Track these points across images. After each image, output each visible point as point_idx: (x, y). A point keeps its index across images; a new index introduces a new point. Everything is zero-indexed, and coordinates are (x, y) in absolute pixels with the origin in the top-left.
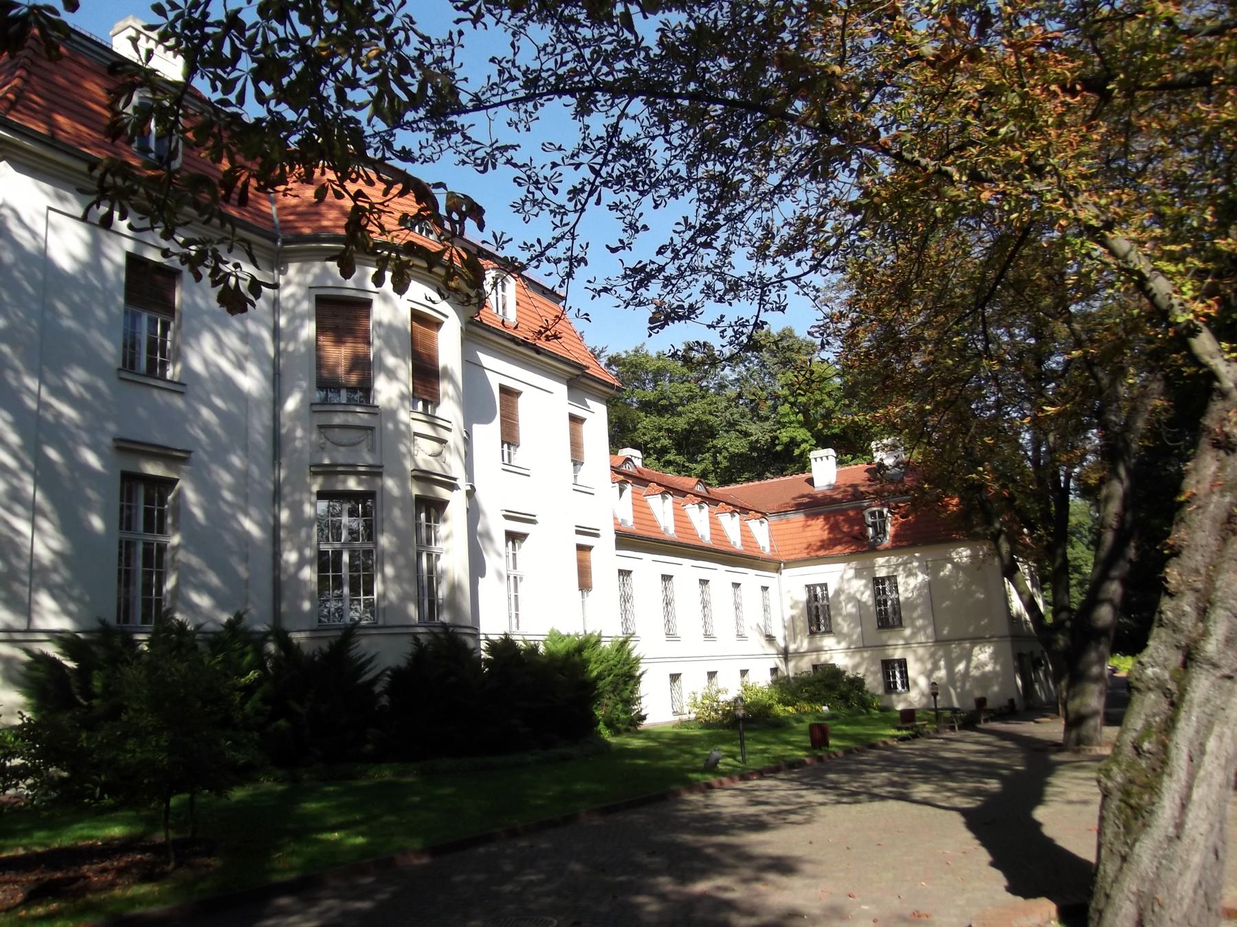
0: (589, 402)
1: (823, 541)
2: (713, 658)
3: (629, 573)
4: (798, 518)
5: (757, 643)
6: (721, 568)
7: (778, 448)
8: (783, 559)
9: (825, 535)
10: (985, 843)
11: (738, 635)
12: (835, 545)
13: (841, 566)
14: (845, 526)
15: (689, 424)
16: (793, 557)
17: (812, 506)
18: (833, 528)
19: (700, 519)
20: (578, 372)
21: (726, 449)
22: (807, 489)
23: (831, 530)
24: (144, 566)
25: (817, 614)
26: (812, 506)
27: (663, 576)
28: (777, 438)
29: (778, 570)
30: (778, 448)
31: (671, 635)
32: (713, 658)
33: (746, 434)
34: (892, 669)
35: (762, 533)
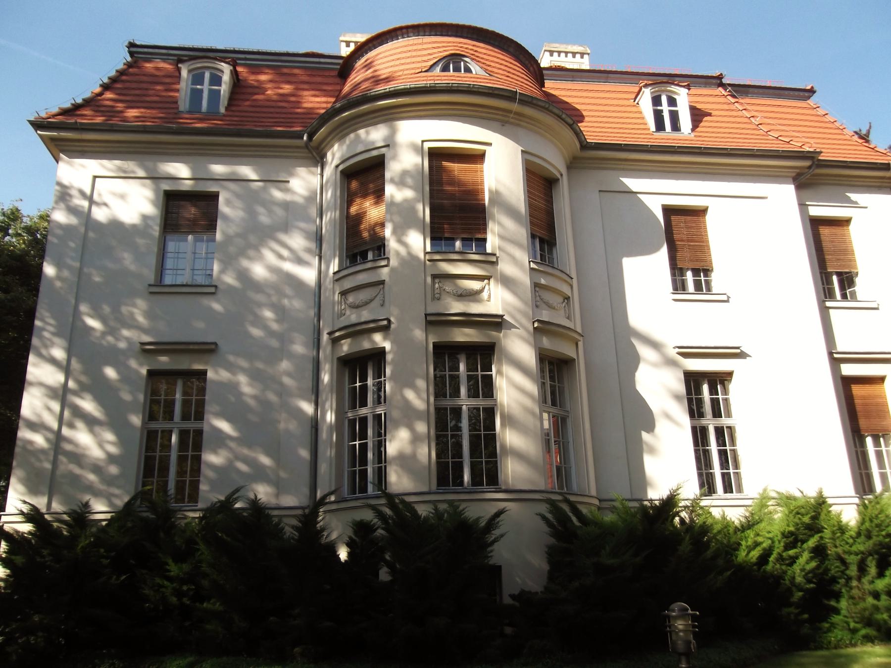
0: (853, 196)
20: (807, 163)
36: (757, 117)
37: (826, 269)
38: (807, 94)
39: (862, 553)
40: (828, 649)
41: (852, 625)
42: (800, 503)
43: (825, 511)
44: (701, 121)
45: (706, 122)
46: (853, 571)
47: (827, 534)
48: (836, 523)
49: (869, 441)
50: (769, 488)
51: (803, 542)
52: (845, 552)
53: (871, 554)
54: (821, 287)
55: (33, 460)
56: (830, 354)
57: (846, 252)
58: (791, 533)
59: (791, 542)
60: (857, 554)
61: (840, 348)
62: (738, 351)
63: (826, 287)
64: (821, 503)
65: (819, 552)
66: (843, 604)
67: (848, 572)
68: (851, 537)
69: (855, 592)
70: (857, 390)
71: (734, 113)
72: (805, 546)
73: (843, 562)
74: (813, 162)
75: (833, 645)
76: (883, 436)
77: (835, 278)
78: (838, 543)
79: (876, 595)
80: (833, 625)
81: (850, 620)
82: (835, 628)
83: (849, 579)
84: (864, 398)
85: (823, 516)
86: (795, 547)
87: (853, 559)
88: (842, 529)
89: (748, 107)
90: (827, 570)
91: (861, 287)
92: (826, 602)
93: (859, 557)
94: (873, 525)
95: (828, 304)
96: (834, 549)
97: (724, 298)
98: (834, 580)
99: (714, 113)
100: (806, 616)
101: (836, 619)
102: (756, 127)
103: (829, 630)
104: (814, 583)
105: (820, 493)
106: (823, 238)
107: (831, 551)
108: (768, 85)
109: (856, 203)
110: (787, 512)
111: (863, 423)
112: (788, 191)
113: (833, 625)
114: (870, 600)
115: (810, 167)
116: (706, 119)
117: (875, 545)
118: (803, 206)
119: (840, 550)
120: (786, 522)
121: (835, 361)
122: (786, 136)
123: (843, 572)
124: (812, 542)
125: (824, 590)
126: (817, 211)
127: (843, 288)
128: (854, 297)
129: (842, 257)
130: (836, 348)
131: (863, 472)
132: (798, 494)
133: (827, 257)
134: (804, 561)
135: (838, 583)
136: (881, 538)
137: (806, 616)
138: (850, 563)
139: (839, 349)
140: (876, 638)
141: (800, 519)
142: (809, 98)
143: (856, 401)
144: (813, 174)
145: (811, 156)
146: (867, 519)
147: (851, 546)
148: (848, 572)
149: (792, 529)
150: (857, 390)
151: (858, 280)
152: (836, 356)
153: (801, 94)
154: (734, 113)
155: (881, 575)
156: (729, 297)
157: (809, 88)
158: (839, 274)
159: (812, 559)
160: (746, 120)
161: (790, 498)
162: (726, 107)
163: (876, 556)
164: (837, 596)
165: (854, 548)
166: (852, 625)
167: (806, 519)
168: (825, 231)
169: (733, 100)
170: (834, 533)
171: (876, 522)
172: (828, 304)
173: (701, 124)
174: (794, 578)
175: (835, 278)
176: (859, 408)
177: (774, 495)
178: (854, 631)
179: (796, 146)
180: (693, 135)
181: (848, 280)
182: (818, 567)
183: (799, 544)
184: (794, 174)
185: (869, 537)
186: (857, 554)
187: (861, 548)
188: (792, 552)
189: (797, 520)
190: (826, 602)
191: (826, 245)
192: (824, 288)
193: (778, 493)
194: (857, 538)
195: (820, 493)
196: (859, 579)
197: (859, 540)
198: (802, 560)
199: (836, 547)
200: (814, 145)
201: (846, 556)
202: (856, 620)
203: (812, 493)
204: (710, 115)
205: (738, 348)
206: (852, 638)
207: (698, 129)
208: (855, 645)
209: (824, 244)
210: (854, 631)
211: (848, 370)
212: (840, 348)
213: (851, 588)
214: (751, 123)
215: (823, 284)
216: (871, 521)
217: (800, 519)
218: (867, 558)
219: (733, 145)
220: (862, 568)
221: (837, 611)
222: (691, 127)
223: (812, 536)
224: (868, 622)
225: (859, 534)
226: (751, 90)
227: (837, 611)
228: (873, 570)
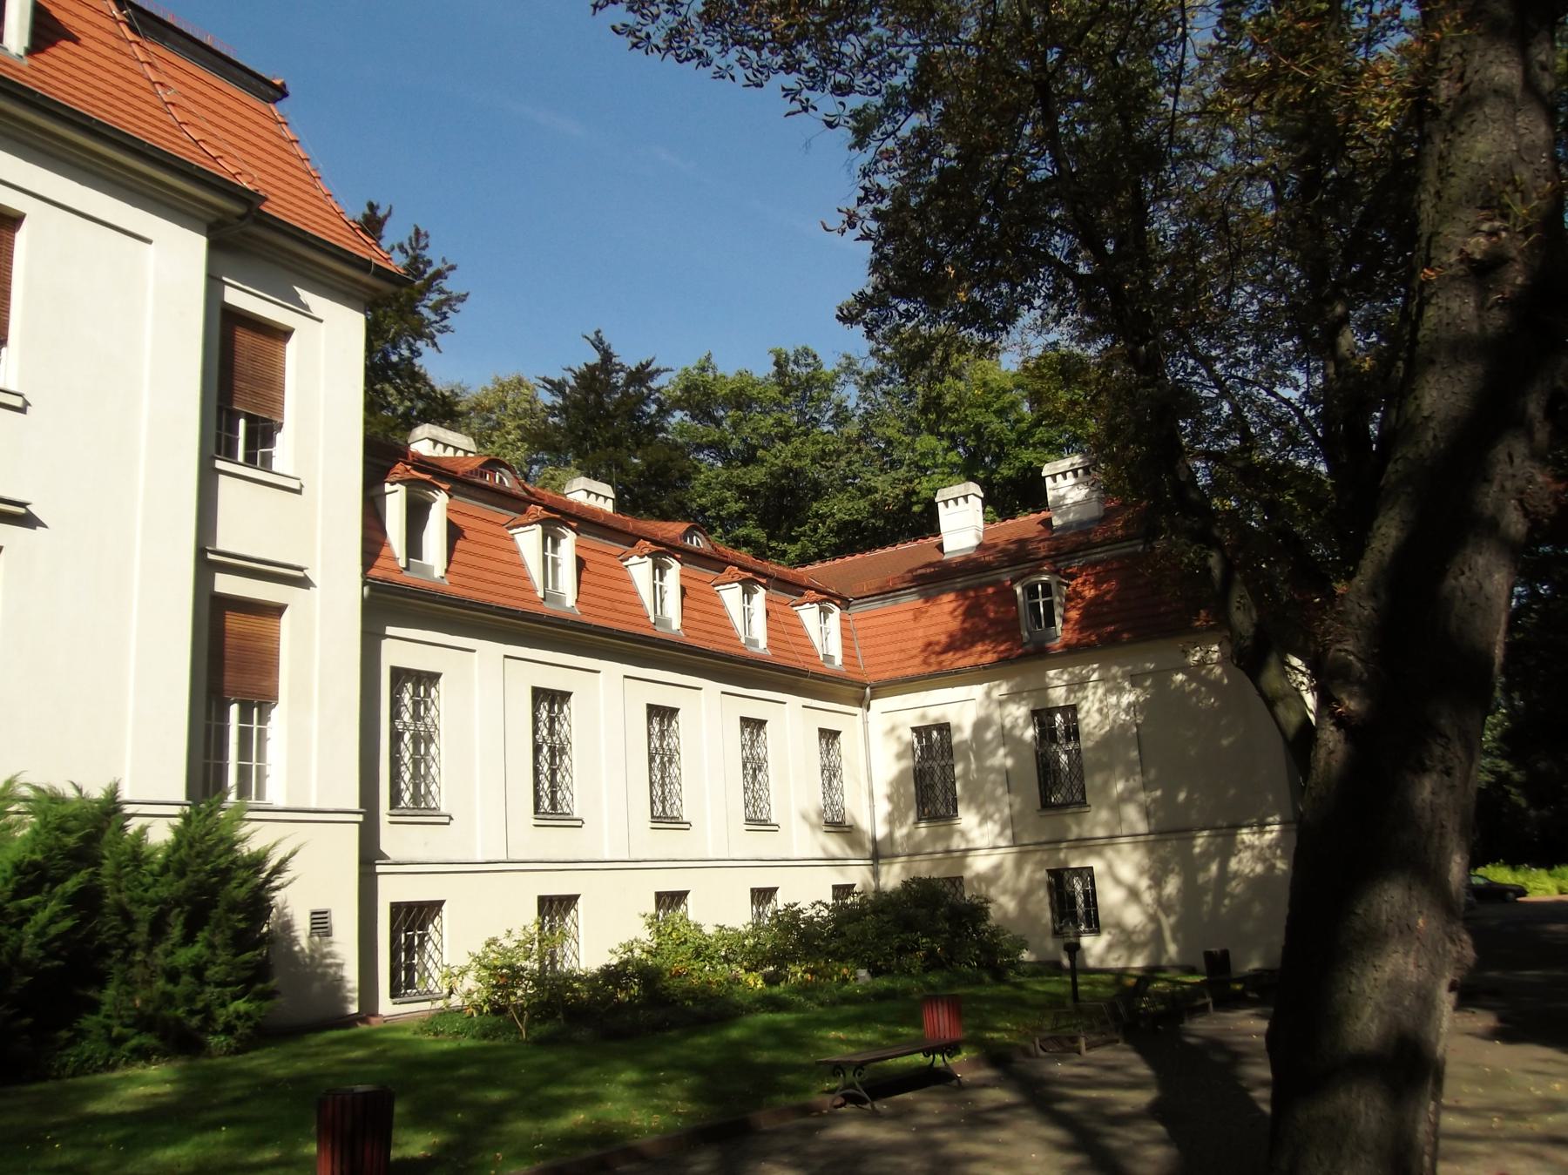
0: (306, 296)
1: (951, 636)
2: (674, 864)
3: (761, 724)
4: (911, 601)
5: (807, 841)
6: (712, 688)
7: (916, 508)
8: (870, 680)
9: (954, 625)
10: (1292, 905)
11: (749, 820)
12: (973, 644)
13: (978, 691)
14: (995, 618)
15: (771, 474)
16: (887, 676)
17: (936, 578)
18: (972, 611)
19: (747, 615)
20: (238, 209)
21: (833, 515)
22: (935, 557)
23: (968, 614)
24: (241, 721)
25: (932, 777)
26: (936, 578)
27: (822, 732)
28: (914, 492)
29: (862, 702)
30: (916, 508)
31: (665, 817)
32: (674, 864)
33: (868, 491)
34: (1071, 904)
35: (824, 633)
36: (170, 88)
37: (231, 403)
38: (271, 92)
39: (164, 901)
40: (58, 1078)
41: (116, 1031)
42: (69, 810)
43: (114, 827)
44: (53, 44)
45: (62, 50)
46: (141, 934)
47: (108, 866)
48: (129, 849)
49: (234, 710)
50: (23, 779)
51: (57, 881)
52: (132, 900)
53: (178, 903)
54: (213, 431)
55: (1122, 1010)
56: (201, 552)
57: (271, 385)
58: (34, 865)
59: (30, 883)
60: (153, 904)
61: (221, 545)
62: (22, 510)
63: (224, 434)
64: (111, 810)
65: (87, 901)
66: (110, 994)
67: (131, 937)
68: (152, 874)
69: (137, 971)
70: (233, 622)
71: (126, 61)
72: (59, 889)
73: (128, 919)
74: (249, 211)
75: (69, 1071)
76: (260, 706)
77: (242, 423)
78: (123, 884)
79: (173, 976)
80: (82, 1034)
81: (115, 1022)
82: (84, 1038)
83: (132, 948)
84: (242, 636)
85: (108, 835)
86: (37, 891)
87: (144, 913)
88: (137, 855)
89: (157, 63)
90: (94, 933)
91: (284, 451)
92: (81, 992)
93: (156, 909)
94: (193, 853)
95: (220, 464)
96: (116, 896)
97: (18, 402)
98: (104, 951)
99: (85, 41)
100: (27, 1021)
101: (89, 1022)
102: (161, 105)
103: (71, 1042)
104: (62, 958)
105: (113, 792)
106: (238, 348)
107: (110, 899)
108: (224, 52)
109: (306, 307)
110: (37, 827)
111: (229, 678)
112: (194, 246)
113: (82, 1034)
114: (161, 984)
115: (241, 218)
116: (64, 44)
117: (189, 887)
118: (214, 283)
119: (124, 897)
120: (30, 845)
121: (207, 563)
122: (217, 148)
123: (122, 937)
124: (71, 885)
125: (78, 967)
126: (235, 297)
127: (251, 445)
128: (266, 464)
129: (261, 391)
130: (214, 542)
131: (212, 762)
132: (71, 793)
133: (237, 383)
134: (48, 913)
135: (110, 956)
136: (202, 876)
137: (27, 1021)
138: (137, 921)
139: (220, 546)
140: (155, 1050)
141: (57, 838)
142: (275, 101)
143: (228, 641)
144: (245, 234)
145: (250, 200)
146: (185, 843)
147: (146, 890)
148: (131, 937)
149: (38, 857)
150: (233, 622)
151: (279, 437)
152: (211, 556)
153: (263, 87)
154: (126, 61)
155: (188, 939)
156: (27, 404)
157: (278, 82)
158: (251, 419)
159: (66, 913)
160: (147, 85)
161: (56, 799)
162: (113, 42)
163: (187, 908)
164: (101, 981)
165: (151, 894)
166: (116, 1031)
167: (71, 841)
168: (244, 338)
169: (130, 36)
170: (119, 866)
171: (198, 847)
172: (220, 464)
173: (53, 50)
174: (19, 950)
175: (242, 423)
176: (229, 652)
177: (26, 792)
178: (119, 1041)
179: (226, 169)
180: (26, 61)
181: (263, 433)
182: (74, 929)
183: (47, 885)
184: (211, 219)
185: (181, 874)
186: (153, 904)
187: (164, 892)
188: (26, 902)
189: (51, 842)
190: (81, 992)
191: (241, 362)
192: (219, 436)
193: (36, 789)
194: (161, 875)
195: (113, 792)
196: (149, 948)
197: (162, 880)
198: (42, 916)
199: (119, 891)
200: (259, 183)
201: (133, 908)
202: (127, 1021)
203: (96, 792)
204: (76, 40)
205: (23, 505)
206: (111, 1055)
207: (42, 57)
208: (113, 1068)
209: (239, 360)
210: (119, 1041)
211: (225, 584)
212: (221, 545)
213: (132, 965)
214: (156, 94)
215: (219, 428)
216: (191, 846)
217: (57, 838)
218: (171, 910)
219: (107, 119)
220: (158, 928)
221: (94, 1006)
222: (26, 43)
223: (77, 871)
224: (144, 1023)
225: (165, 868)
226: (172, 35)
227: (94, 1006)
228: (176, 933)
